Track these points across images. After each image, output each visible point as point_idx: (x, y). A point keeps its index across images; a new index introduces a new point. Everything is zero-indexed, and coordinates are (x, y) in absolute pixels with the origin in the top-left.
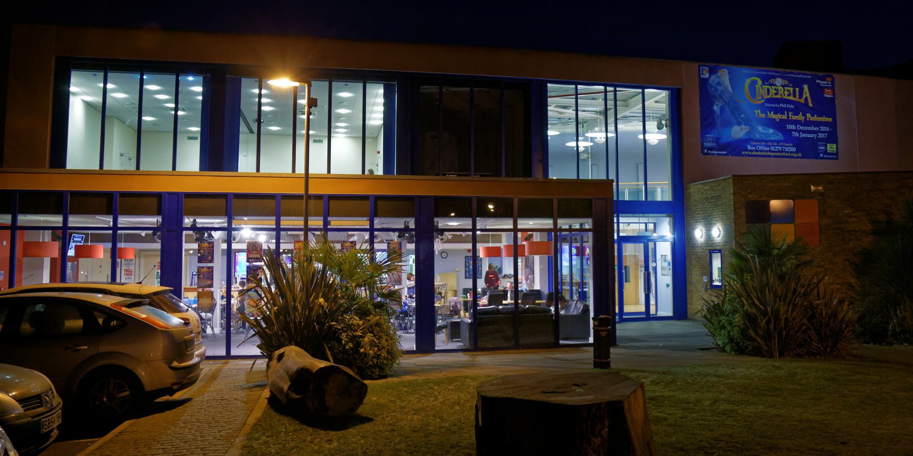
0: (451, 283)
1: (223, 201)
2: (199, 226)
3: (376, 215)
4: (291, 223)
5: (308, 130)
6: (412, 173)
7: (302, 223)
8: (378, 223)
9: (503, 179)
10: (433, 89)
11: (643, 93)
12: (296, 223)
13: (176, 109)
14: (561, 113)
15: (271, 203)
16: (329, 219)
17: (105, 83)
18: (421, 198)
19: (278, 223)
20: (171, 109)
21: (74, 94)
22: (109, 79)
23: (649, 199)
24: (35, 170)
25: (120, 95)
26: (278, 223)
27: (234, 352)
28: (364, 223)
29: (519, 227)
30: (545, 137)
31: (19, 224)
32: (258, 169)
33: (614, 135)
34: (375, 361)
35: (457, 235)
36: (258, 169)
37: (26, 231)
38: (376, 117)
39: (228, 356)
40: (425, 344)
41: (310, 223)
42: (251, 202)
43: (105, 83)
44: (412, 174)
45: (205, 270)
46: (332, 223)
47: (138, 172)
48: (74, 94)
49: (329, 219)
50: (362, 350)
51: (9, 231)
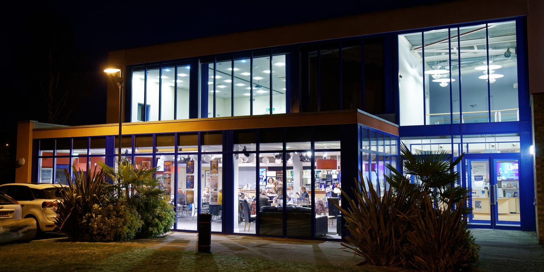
0: (244, 188)
2: (247, 150)
3: (203, 144)
8: (204, 149)
11: (423, 34)
15: (151, 139)
17: (233, 67)
18: (226, 131)
19: (200, 149)
22: (163, 73)
26: (200, 149)
30: (286, 88)
32: (175, 118)
36: (175, 118)
40: (228, 228)
43: (233, 67)
45: (190, 177)
46: (159, 150)
49: (157, 148)
51: (260, 150)
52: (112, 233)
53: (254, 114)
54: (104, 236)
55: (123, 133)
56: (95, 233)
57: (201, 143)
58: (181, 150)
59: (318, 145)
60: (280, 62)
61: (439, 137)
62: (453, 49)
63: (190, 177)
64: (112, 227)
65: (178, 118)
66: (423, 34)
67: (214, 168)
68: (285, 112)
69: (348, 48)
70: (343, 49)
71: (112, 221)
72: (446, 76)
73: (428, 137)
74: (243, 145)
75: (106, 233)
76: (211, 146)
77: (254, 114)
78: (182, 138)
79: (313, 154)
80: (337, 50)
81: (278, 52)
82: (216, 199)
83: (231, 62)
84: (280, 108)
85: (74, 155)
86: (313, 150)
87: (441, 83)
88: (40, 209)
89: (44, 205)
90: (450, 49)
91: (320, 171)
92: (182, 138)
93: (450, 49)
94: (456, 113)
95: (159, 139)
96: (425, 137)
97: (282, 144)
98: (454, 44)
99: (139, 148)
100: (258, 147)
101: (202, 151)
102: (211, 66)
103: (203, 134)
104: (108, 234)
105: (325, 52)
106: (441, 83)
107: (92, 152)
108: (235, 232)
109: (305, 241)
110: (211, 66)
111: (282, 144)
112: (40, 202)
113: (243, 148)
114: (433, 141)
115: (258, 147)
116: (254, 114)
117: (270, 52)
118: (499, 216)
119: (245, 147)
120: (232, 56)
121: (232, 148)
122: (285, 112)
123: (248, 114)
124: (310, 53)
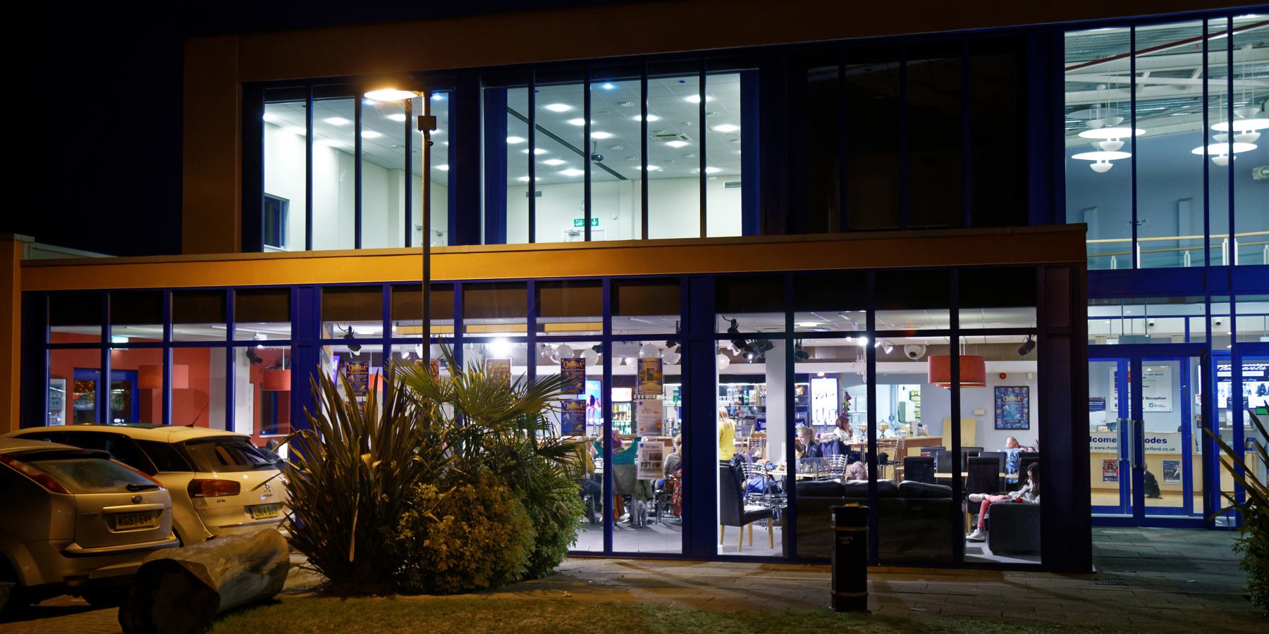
1: (284, 298)
2: (741, 330)
3: (617, 314)
4: (556, 327)
5: (644, 164)
6: (790, 231)
7: (420, 329)
8: (620, 326)
9: (483, 246)
10: (831, 72)
11: (1133, 32)
12: (411, 329)
13: (587, 129)
14: (1183, 87)
15: (523, 294)
16: (466, 321)
18: (690, 277)
19: (607, 326)
20: (598, 129)
21: (274, 126)
23: (1212, 264)
24: (214, 256)
25: (558, 108)
26: (607, 326)
27: (617, 548)
28: (594, 326)
29: (615, 331)
31: (236, 338)
33: (1214, 127)
34: (452, 562)
35: (755, 344)
37: (212, 349)
38: (728, 127)
39: (608, 552)
41: (433, 329)
42: (506, 293)
44: (789, 232)
45: (573, 405)
46: (547, 327)
47: (309, 254)
48: (274, 126)
49: (466, 321)
50: (427, 543)
52: (488, 565)
53: (651, 237)
54: (466, 576)
55: (435, 276)
56: (443, 566)
57: (610, 310)
58: (542, 328)
59: (884, 320)
60: (726, 92)
61: (1166, 299)
62: (1141, 75)
63: (573, 405)
64: (487, 549)
65: (366, 244)
66: (1133, 32)
67: (651, 378)
68: (740, 234)
69: (920, 61)
70: (909, 63)
71: (481, 532)
72: (1215, 137)
73: (1137, 300)
74: (730, 317)
75: (474, 566)
76: (632, 319)
77: (652, 235)
78: (470, 295)
79: (872, 342)
80: (897, 65)
81: (722, 64)
82: (659, 465)
83: (582, 86)
84: (727, 218)
85: (116, 340)
86: (872, 332)
87: (1095, 162)
88: (186, 504)
89: (195, 488)
90: (1133, 75)
91: (752, 388)
92: (623, 291)
93: (1133, 75)
94: (1220, 238)
95: (471, 297)
96: (1129, 300)
97: (784, 315)
98: (1218, 58)
99: (401, 322)
100: (790, 323)
101: (614, 333)
102: (516, 98)
103: (616, 282)
104: (477, 570)
105: (854, 71)
106: (1095, 162)
107: (181, 331)
108: (720, 552)
109: (939, 570)
110: (516, 98)
111: (784, 315)
112: (182, 480)
113: (729, 325)
114: (1129, 310)
115: (954, 321)
116: (651, 237)
117: (700, 64)
118: (1093, 495)
119: (734, 322)
120: (579, 71)
121: (317, 330)
122: (740, 234)
123: (696, 234)
124: (810, 71)
